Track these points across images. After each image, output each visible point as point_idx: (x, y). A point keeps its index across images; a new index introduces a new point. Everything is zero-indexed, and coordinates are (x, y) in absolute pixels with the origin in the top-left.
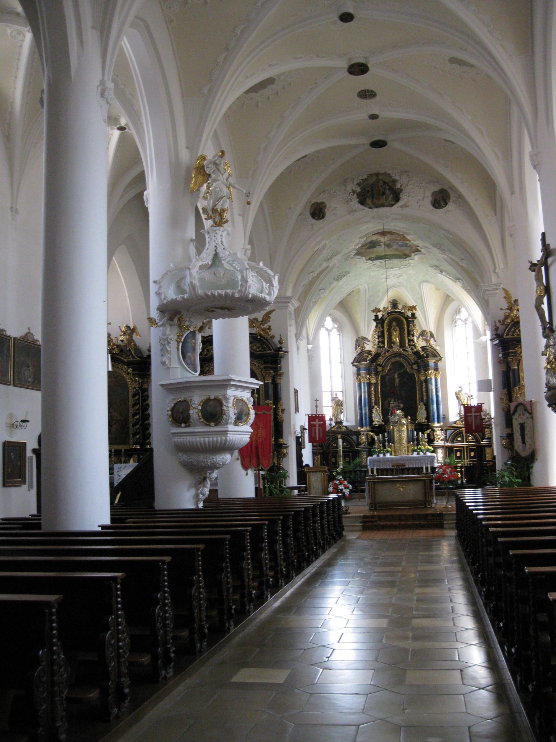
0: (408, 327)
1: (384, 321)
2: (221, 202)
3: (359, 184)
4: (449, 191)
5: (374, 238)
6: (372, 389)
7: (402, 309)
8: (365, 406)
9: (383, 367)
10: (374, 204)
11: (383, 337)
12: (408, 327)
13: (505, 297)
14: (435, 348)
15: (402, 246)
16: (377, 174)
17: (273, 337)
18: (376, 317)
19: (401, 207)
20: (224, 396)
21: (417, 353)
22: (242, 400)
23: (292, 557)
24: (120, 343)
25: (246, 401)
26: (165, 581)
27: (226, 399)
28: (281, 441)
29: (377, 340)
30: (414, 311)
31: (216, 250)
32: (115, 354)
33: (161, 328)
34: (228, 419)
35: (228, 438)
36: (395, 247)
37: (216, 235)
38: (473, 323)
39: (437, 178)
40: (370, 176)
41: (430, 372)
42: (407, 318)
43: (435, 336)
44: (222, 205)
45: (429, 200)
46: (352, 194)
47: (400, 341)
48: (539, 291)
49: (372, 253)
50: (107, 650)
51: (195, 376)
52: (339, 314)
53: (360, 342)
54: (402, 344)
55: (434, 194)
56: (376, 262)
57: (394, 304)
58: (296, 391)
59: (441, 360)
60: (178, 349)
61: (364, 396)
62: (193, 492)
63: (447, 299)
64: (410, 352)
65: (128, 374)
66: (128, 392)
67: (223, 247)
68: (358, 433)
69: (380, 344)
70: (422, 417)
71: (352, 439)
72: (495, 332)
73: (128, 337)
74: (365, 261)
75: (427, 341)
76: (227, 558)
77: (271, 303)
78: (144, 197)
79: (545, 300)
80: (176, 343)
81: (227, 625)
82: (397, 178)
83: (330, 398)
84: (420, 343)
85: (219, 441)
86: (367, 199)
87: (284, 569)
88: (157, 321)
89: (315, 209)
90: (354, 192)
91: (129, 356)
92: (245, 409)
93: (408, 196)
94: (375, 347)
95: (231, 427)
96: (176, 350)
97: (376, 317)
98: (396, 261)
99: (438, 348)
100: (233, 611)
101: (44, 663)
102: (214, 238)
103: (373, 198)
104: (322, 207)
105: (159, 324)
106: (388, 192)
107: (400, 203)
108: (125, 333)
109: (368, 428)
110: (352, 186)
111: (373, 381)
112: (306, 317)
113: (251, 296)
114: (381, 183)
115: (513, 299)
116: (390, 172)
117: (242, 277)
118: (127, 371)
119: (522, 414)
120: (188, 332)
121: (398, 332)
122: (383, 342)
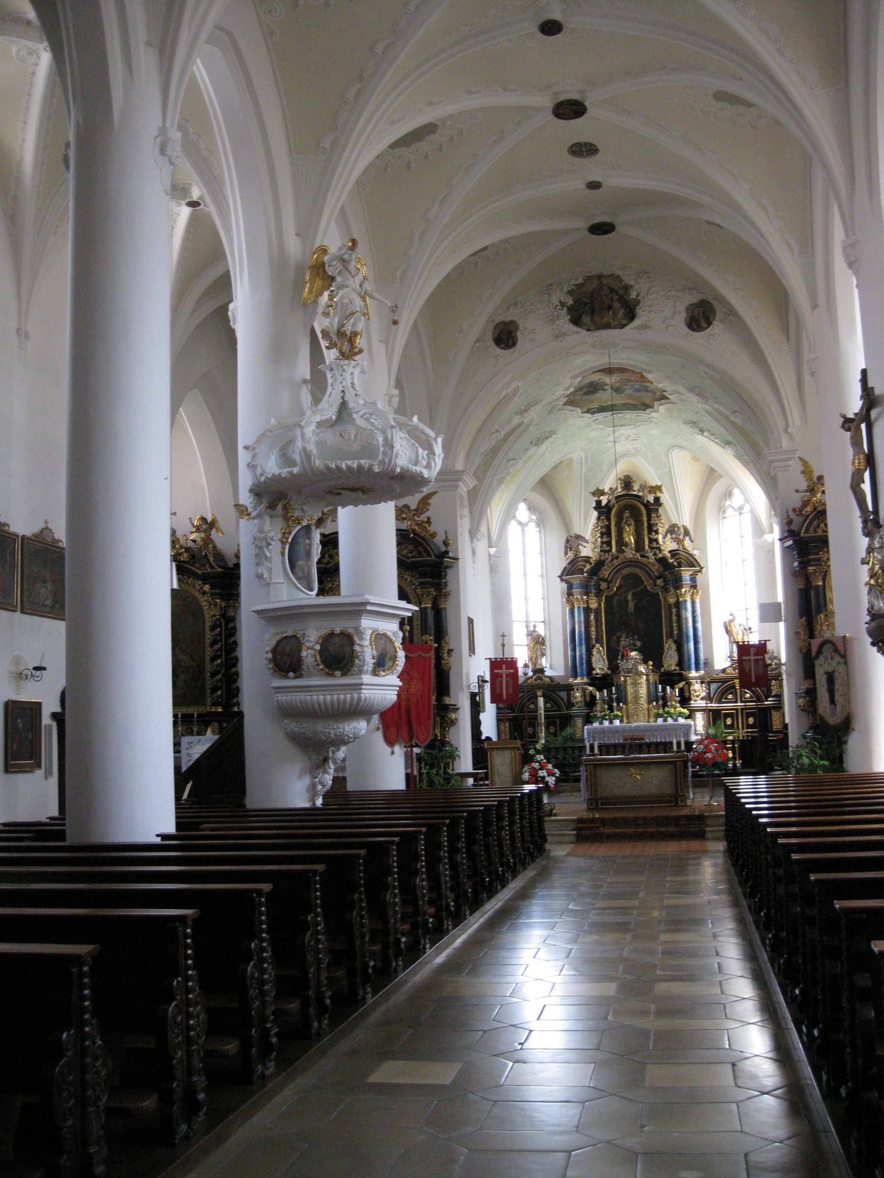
0: (649, 519)
1: (611, 509)
2: (352, 321)
3: (570, 293)
4: (714, 303)
5: (595, 378)
6: (592, 617)
7: (639, 491)
8: (581, 644)
9: (609, 583)
10: (595, 324)
11: (609, 536)
12: (649, 519)
13: (803, 472)
14: (692, 552)
15: (638, 391)
16: (600, 277)
17: (434, 535)
18: (599, 503)
19: (638, 328)
20: (357, 629)
21: (663, 561)
22: (385, 635)
23: (465, 884)
24: (191, 544)
25: (392, 637)
26: (262, 922)
27: (360, 633)
28: (447, 701)
29: (599, 540)
30: (659, 494)
31: (343, 398)
32: (184, 562)
33: (256, 521)
34: (363, 666)
35: (363, 695)
36: (628, 391)
37: (343, 373)
38: (753, 513)
39: (696, 283)
40: (589, 279)
41: (683, 590)
42: (647, 505)
43: (692, 533)
44: (354, 325)
45: (681, 317)
46: (560, 307)
47: (636, 542)
48: (857, 461)
49: (592, 401)
50: (170, 1032)
51: (310, 597)
52: (539, 499)
53: (572, 542)
54: (639, 546)
55: (690, 308)
56: (598, 416)
57: (627, 482)
58: (471, 621)
59: (700, 571)
60: (283, 555)
61: (579, 628)
62: (306, 780)
63: (711, 475)
64: (652, 559)
65: (204, 593)
66: (204, 622)
67: (355, 392)
68: (569, 688)
69: (605, 546)
70: (670, 661)
71: (559, 696)
72: (786, 528)
73: (203, 535)
74: (581, 414)
75: (679, 542)
76: (361, 885)
77: (430, 481)
78: (230, 313)
79: (867, 476)
80: (280, 544)
81: (361, 992)
82: (632, 282)
83: (525, 632)
84: (668, 545)
85: (348, 700)
86: (584, 316)
87: (452, 904)
88: (250, 510)
89: (501, 332)
90: (563, 304)
91: (204, 565)
92: (389, 649)
93: (649, 312)
94: (596, 550)
95: (367, 678)
96: (280, 556)
97: (599, 503)
98: (630, 415)
99: (696, 553)
100: (370, 971)
101: (70, 1053)
102: (340, 379)
103: (592, 314)
104: (511, 328)
105: (253, 514)
106: (616, 305)
107: (636, 322)
108: (198, 529)
109: (585, 680)
110: (560, 296)
111: (594, 605)
112: (486, 503)
113: (398, 470)
114: (605, 291)
115: (816, 475)
116: (620, 273)
117: (385, 439)
118: (202, 588)
119: (829, 657)
120: (299, 527)
121: (632, 527)
122: (609, 544)
